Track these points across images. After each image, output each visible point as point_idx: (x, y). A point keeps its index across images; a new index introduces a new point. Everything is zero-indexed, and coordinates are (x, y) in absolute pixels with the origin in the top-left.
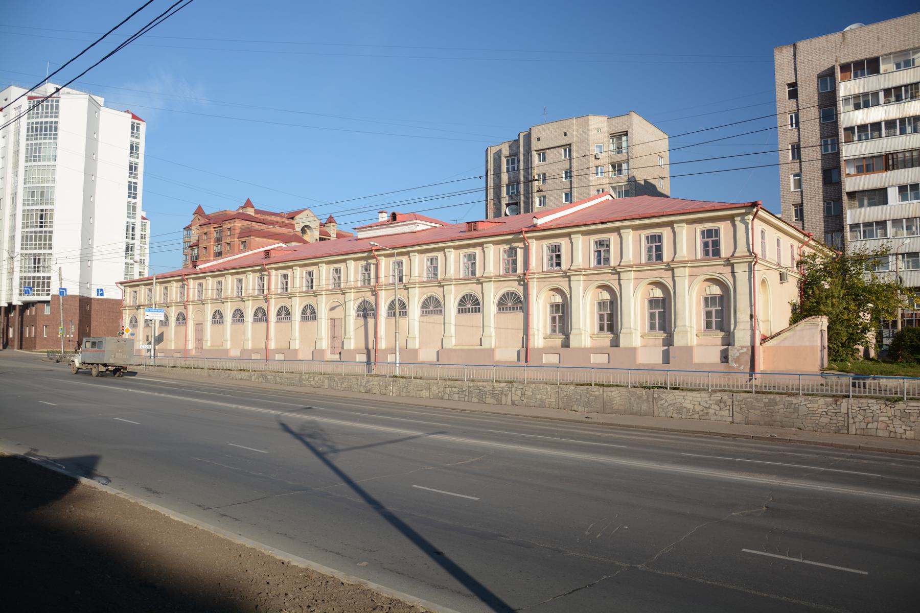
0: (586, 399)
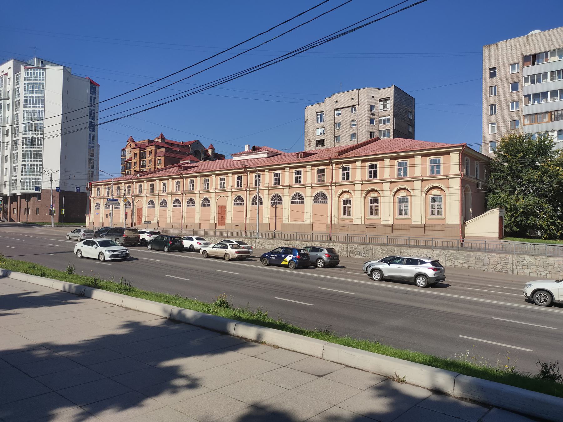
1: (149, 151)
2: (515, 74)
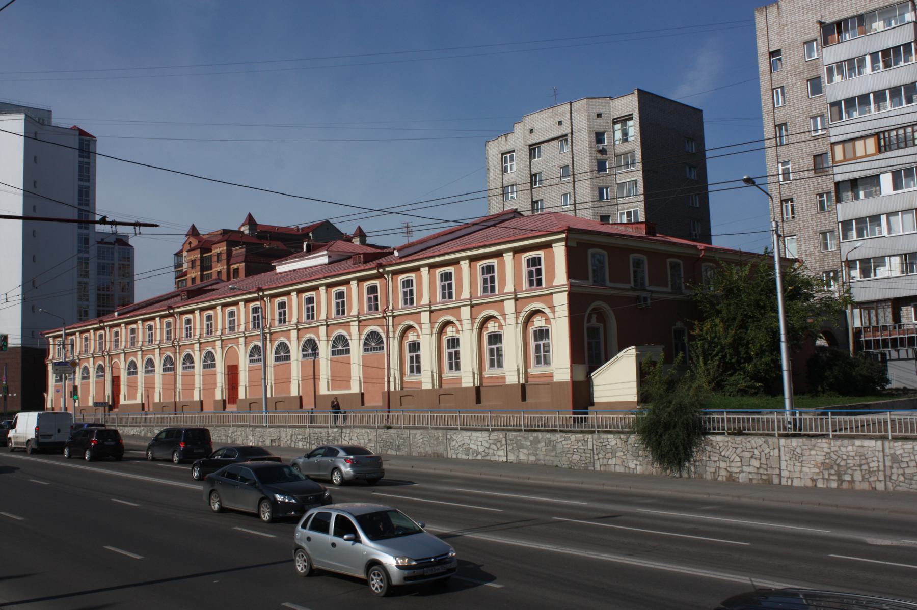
0: (397, 443)
2: (814, 61)
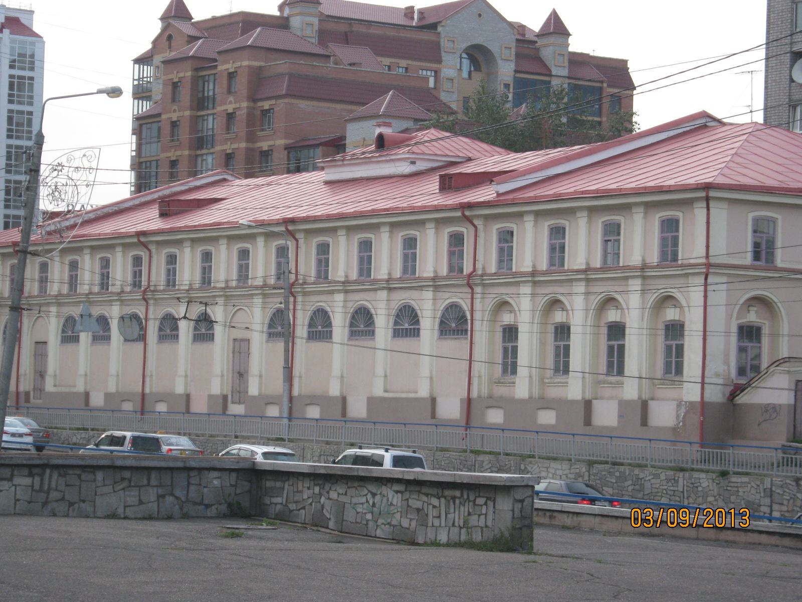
1: (225, 74)
